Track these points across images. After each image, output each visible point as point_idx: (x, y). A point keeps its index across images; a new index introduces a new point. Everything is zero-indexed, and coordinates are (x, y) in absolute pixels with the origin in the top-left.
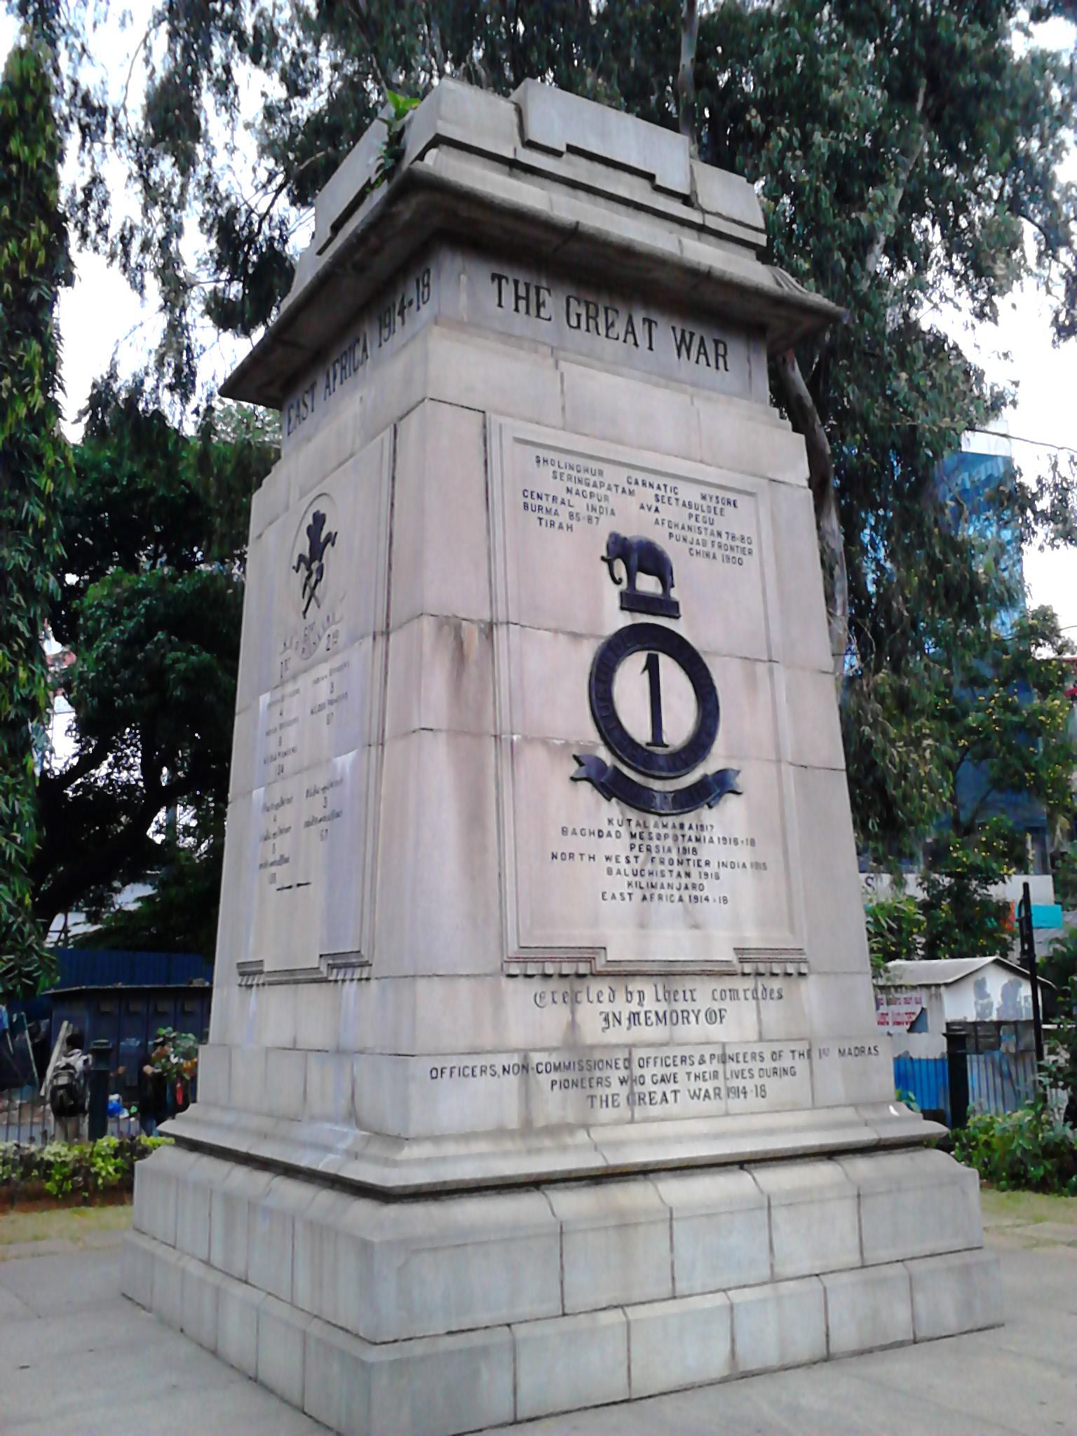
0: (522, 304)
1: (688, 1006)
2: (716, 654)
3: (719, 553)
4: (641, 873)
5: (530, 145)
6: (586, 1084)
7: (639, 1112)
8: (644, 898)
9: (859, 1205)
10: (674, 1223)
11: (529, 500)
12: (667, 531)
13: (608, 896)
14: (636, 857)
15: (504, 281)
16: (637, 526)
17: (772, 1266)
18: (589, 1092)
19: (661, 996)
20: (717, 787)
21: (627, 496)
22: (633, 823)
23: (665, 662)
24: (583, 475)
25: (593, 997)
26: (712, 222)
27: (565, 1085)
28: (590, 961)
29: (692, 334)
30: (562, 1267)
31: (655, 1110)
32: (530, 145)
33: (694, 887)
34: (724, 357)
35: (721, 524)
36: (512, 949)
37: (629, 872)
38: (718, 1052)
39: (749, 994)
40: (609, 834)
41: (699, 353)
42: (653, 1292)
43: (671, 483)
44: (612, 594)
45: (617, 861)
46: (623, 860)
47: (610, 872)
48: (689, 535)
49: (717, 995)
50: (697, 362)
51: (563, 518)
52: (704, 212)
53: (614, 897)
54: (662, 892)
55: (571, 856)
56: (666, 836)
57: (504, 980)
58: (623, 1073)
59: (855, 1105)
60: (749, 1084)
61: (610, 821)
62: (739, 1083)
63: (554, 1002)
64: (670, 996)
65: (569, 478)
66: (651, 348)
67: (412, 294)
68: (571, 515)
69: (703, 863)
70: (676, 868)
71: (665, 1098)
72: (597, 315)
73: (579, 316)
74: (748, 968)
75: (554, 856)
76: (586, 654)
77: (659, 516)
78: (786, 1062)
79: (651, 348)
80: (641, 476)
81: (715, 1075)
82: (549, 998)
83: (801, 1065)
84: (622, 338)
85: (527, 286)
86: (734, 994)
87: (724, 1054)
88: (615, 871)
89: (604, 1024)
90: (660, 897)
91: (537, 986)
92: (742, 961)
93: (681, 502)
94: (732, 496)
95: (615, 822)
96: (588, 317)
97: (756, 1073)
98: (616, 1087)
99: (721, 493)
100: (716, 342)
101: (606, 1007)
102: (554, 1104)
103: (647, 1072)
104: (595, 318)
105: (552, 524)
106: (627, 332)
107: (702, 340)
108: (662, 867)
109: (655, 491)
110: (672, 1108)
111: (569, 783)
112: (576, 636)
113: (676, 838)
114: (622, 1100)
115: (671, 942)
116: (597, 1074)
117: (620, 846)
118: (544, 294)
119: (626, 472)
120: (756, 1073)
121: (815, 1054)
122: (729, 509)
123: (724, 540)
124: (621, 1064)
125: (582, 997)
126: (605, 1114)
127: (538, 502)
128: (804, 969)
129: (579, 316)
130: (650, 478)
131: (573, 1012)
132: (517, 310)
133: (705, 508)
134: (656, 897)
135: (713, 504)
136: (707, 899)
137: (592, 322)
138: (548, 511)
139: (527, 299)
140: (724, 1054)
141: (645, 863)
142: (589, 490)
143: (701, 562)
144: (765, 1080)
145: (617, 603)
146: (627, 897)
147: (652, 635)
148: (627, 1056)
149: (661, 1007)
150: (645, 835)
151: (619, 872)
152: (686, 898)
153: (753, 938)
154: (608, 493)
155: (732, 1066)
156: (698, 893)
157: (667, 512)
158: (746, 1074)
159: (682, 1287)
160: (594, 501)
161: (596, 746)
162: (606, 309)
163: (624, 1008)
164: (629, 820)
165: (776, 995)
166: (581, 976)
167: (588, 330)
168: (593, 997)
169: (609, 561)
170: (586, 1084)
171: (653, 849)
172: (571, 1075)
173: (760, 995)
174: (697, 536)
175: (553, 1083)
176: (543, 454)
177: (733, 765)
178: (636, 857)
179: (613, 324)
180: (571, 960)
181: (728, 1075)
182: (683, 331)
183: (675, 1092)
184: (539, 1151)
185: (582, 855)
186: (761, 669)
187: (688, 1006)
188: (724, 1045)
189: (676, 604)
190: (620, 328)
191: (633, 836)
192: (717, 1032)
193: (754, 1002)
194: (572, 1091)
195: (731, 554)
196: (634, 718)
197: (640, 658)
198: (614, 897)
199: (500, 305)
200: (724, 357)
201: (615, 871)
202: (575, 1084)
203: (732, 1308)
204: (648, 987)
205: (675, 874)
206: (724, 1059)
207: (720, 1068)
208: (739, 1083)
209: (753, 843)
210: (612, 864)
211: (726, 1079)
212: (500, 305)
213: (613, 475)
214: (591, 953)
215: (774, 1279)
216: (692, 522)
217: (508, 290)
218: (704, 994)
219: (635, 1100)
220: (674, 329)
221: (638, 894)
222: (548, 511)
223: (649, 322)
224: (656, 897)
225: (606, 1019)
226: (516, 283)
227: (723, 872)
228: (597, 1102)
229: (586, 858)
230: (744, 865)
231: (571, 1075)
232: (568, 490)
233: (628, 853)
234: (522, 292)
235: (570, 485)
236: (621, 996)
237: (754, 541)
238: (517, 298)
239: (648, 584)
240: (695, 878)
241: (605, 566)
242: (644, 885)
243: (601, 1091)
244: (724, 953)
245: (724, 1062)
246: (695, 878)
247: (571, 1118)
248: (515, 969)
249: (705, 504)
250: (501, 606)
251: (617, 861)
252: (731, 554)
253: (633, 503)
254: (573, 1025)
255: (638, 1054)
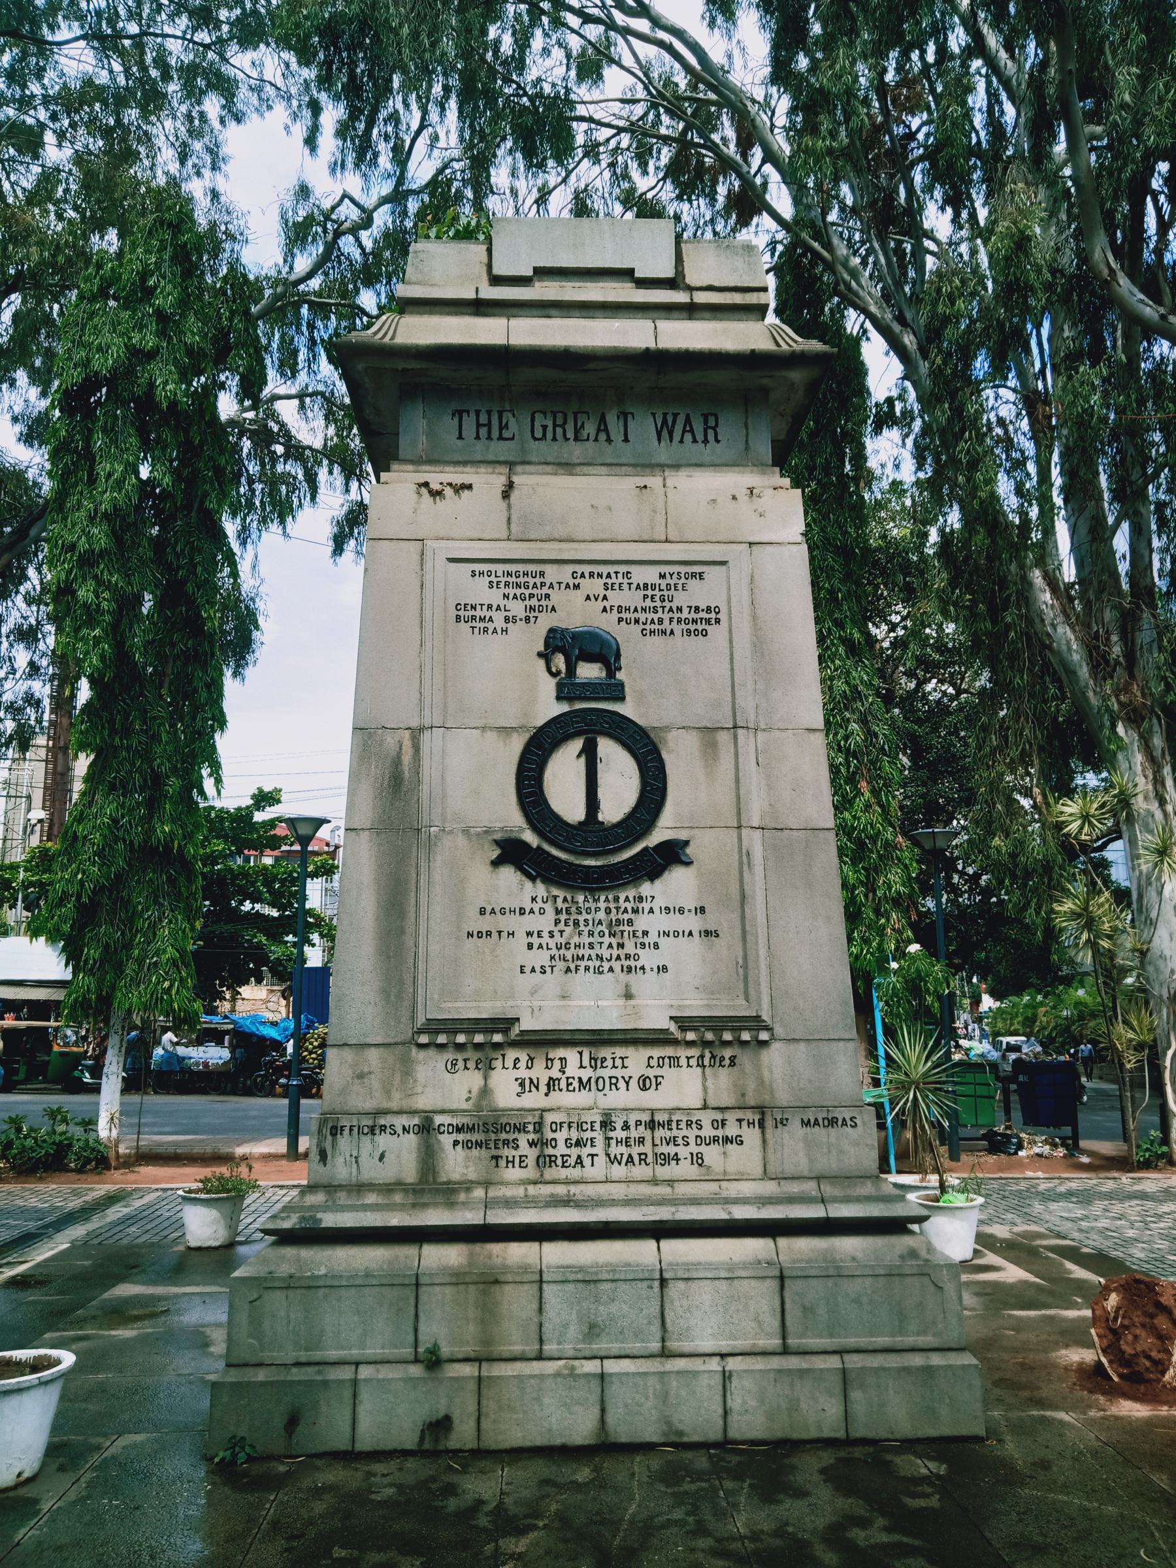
0: (483, 431)
1: (618, 1073)
2: (667, 729)
3: (678, 629)
4: (567, 946)
5: (496, 280)
6: (492, 1145)
7: (550, 1173)
8: (568, 970)
9: (782, 1287)
10: (545, 1286)
11: (461, 613)
12: (615, 615)
13: (528, 969)
14: (561, 932)
15: (465, 415)
16: (576, 612)
17: (663, 1340)
18: (494, 1152)
19: (586, 1062)
20: (672, 854)
21: (571, 592)
22: (559, 900)
23: (607, 748)
24: (522, 580)
25: (509, 1063)
26: (701, 298)
27: (468, 1145)
28: (505, 1031)
29: (675, 416)
30: (417, 1316)
31: (564, 1173)
32: (496, 280)
33: (628, 957)
34: (714, 429)
35: (680, 599)
36: (421, 1021)
37: (552, 945)
38: (645, 1117)
39: (693, 1062)
40: (532, 911)
41: (684, 431)
42: (517, 1348)
43: (623, 569)
44: (549, 686)
45: (539, 936)
46: (545, 934)
47: (530, 946)
48: (642, 617)
49: (654, 1062)
50: (681, 441)
51: (499, 623)
52: (691, 289)
53: (533, 970)
54: (590, 963)
55: (489, 934)
56: (597, 910)
57: (414, 1050)
58: (531, 1136)
59: (818, 1178)
60: (683, 1152)
61: (534, 899)
62: (671, 1150)
63: (466, 1068)
64: (595, 1062)
65: (507, 584)
66: (626, 440)
67: (643, 427)
68: (507, 620)
69: (639, 934)
70: (607, 940)
71: (579, 1161)
72: (565, 422)
73: (545, 427)
74: (691, 1036)
75: (470, 935)
76: (517, 744)
77: (607, 604)
78: (731, 1130)
79: (626, 440)
80: (587, 569)
81: (641, 1141)
82: (461, 1064)
83: (752, 1136)
84: (592, 437)
85: (489, 413)
86: (674, 1061)
87: (652, 1121)
88: (536, 946)
89: (519, 1089)
90: (587, 969)
91: (450, 1055)
92: (683, 1029)
93: (634, 586)
94: (697, 569)
95: (539, 899)
96: (555, 426)
97: (692, 1141)
98: (524, 1148)
99: (683, 569)
100: (705, 418)
101: (523, 1073)
102: (456, 1162)
103: (561, 1136)
104: (563, 426)
105: (486, 630)
106: (598, 431)
107: (688, 421)
108: (591, 940)
109: (604, 580)
110: (589, 1172)
111: (490, 868)
112: (505, 731)
113: (608, 911)
114: (531, 1161)
115: (593, 1003)
116: (504, 1136)
117: (545, 922)
118: (507, 416)
119: (570, 568)
120: (692, 1141)
121: (769, 1123)
122: (693, 583)
123: (685, 614)
124: (530, 1128)
125: (498, 1064)
126: (513, 1173)
127: (473, 613)
128: (764, 1036)
129: (545, 427)
130: (596, 569)
131: (486, 1078)
132: (478, 437)
133: (663, 587)
134: (582, 969)
135: (675, 580)
136: (643, 968)
137: (559, 430)
138: (482, 619)
139: (489, 425)
140: (652, 1121)
141: (571, 936)
142: (527, 592)
143: (657, 640)
144: (703, 1149)
145: (553, 693)
146: (548, 970)
147: (592, 716)
148: (537, 1119)
149: (586, 1074)
150: (573, 909)
151: (540, 946)
152: (617, 968)
153: (696, 1006)
154: (550, 592)
155: (660, 1133)
156: (632, 963)
157: (615, 598)
158: (680, 1141)
159: (550, 1348)
160: (534, 602)
161: (522, 830)
162: (576, 415)
163: (540, 1072)
164: (555, 897)
165: (727, 1062)
166: (497, 1046)
167: (554, 439)
168: (509, 1063)
169: (546, 656)
170: (674, 1125)
171: (582, 923)
172: (475, 1137)
173: (706, 1062)
174: (651, 616)
175: (456, 1143)
176: (478, 567)
177: (683, 835)
178: (561, 932)
179: (583, 426)
180: (485, 1031)
181: (658, 1142)
182: (665, 415)
183: (593, 1156)
184: (425, 1206)
185: (500, 932)
186: (723, 737)
187: (618, 1073)
188: (653, 1111)
189: (621, 685)
190: (590, 428)
191: (558, 912)
192: (652, 1099)
193: (699, 1070)
194: (475, 1152)
195: (692, 627)
196: (567, 801)
197: (577, 744)
198: (533, 970)
199: (460, 437)
200: (714, 429)
201: (536, 946)
202: (479, 1144)
203: (480, 1378)
204: (571, 1055)
205: (605, 946)
206: (652, 1125)
207: (648, 1134)
208: (671, 1150)
209: (703, 910)
210: (535, 940)
211: (654, 1145)
212: (460, 437)
213: (553, 573)
214: (505, 1024)
215: (665, 1353)
216: (648, 603)
217: (469, 423)
218: (637, 1060)
219: (546, 1161)
220: (654, 415)
221: (561, 965)
222: (482, 619)
223: (624, 416)
224: (582, 969)
225: (522, 1085)
226: (478, 413)
227: (663, 941)
228: (503, 1163)
229: (504, 935)
230: (690, 934)
231: (475, 1137)
232: (506, 596)
233: (552, 928)
234: (483, 419)
235: (507, 591)
236: (540, 1064)
237: (724, 610)
238: (479, 425)
239: (589, 672)
240: (629, 948)
241: (542, 663)
242: (569, 957)
243: (507, 1152)
244: (657, 1019)
245: (653, 1129)
246: (629, 948)
247: (472, 1176)
248: (424, 1039)
249: (663, 583)
250: (427, 712)
251: (539, 936)
252: (692, 627)
253: (579, 595)
254: (485, 1091)
255: (549, 1118)
